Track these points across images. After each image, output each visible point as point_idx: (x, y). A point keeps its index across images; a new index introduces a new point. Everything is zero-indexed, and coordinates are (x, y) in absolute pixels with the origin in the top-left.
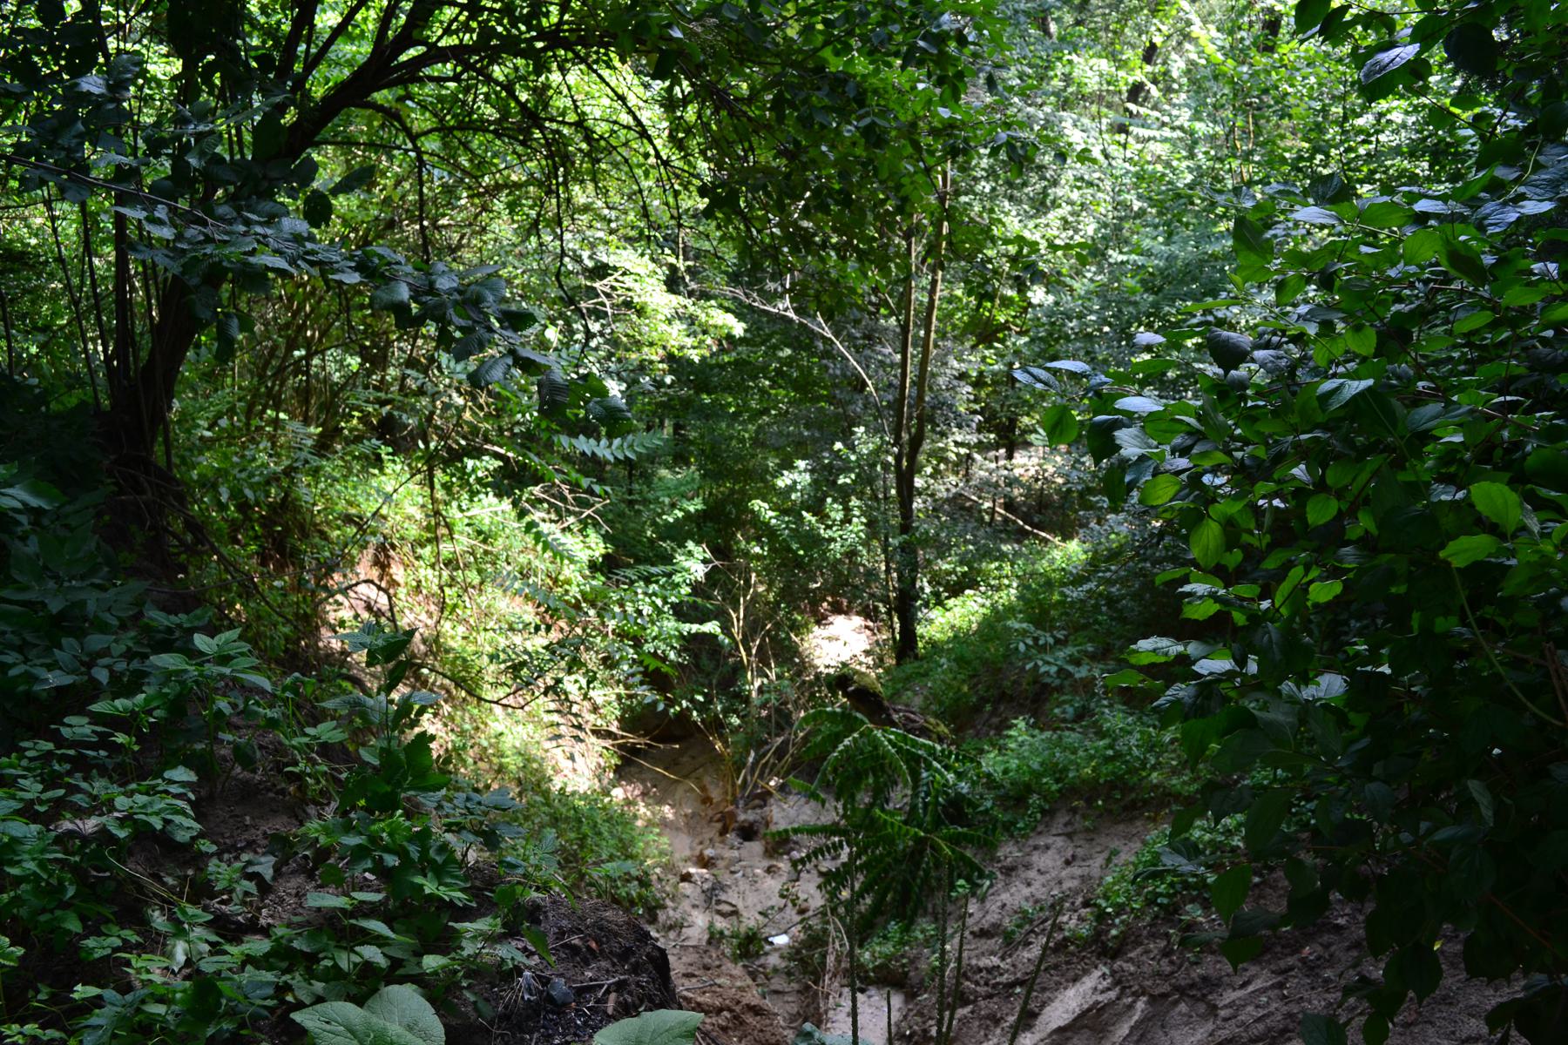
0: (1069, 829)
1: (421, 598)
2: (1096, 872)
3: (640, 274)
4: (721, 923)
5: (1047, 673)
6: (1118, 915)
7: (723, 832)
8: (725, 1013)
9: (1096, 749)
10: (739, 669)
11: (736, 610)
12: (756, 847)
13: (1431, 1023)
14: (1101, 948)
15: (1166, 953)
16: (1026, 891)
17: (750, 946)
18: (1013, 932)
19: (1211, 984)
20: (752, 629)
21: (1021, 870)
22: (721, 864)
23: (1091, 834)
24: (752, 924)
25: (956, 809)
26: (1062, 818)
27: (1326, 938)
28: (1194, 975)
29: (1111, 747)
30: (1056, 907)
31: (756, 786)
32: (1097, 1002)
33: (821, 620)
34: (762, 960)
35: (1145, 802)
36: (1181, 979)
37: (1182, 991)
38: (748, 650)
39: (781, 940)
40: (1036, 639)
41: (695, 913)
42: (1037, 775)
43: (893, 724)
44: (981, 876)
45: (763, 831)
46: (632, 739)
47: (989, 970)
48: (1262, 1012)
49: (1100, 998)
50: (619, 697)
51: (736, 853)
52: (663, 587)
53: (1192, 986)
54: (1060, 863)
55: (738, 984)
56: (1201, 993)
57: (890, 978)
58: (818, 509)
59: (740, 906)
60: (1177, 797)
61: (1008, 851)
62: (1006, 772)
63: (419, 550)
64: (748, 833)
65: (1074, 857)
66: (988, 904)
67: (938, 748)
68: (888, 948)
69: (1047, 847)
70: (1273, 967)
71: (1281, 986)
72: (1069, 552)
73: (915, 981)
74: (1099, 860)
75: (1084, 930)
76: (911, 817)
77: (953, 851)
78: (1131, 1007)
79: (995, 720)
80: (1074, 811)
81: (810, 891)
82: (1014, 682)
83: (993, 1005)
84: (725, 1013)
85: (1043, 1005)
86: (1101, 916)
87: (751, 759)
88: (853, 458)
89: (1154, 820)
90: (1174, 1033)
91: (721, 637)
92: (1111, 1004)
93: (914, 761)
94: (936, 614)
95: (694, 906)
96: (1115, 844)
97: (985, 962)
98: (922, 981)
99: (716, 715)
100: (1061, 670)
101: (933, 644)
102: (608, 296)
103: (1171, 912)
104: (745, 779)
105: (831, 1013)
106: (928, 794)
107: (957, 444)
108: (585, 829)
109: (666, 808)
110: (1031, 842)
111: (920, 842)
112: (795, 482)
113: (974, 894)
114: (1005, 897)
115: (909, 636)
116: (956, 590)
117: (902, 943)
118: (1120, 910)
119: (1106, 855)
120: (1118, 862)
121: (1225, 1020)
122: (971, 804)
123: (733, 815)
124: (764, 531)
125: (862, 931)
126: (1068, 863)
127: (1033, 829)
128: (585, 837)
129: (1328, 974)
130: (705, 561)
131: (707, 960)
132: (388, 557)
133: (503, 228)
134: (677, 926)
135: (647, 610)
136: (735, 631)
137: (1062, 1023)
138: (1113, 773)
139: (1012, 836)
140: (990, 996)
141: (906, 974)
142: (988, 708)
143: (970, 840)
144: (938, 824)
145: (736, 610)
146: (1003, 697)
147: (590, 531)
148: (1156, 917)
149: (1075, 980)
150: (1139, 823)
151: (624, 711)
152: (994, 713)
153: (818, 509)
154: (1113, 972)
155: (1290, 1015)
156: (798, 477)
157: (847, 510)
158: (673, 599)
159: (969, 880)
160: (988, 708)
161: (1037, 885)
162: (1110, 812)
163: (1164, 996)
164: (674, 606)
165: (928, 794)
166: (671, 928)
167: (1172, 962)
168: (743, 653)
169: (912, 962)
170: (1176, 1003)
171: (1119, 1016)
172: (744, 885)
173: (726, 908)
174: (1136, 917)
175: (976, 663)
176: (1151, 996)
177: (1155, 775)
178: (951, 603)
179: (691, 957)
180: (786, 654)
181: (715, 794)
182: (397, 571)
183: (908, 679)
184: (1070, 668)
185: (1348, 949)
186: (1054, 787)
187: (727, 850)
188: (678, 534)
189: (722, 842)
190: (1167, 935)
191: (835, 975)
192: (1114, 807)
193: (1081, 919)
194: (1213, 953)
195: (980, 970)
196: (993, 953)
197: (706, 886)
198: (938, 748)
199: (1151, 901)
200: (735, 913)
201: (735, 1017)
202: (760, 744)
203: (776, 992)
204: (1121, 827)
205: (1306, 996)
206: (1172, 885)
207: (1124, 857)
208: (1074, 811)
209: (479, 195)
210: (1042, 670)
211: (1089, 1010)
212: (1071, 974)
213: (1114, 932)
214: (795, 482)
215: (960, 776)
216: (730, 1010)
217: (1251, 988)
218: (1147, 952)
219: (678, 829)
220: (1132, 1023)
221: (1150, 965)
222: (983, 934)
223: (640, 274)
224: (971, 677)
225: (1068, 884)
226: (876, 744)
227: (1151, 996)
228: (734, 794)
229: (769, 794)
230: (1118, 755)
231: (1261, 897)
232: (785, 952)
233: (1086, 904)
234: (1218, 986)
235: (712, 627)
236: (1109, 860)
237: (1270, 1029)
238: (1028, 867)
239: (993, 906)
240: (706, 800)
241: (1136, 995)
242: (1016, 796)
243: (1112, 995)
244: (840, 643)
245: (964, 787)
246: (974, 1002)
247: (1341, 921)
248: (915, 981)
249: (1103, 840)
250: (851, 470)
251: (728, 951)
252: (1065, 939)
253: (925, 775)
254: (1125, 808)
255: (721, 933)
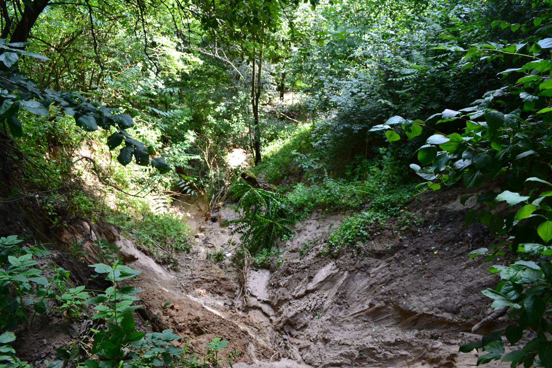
0: (317, 218)
1: (103, 154)
2: (327, 231)
3: (168, 45)
4: (210, 251)
5: (305, 168)
6: (336, 245)
7: (206, 220)
8: (215, 282)
9: (325, 193)
10: (207, 169)
11: (205, 151)
12: (217, 224)
13: (436, 276)
14: (332, 256)
15: (352, 257)
16: (305, 238)
17: (219, 257)
18: (302, 251)
19: (367, 266)
20: (211, 155)
21: (303, 231)
22: (206, 230)
23: (324, 219)
24: (219, 250)
25: (281, 213)
26: (315, 214)
27: (402, 251)
28: (362, 264)
29: (329, 192)
30: (315, 243)
31: (215, 205)
32: (332, 273)
33: (231, 151)
34: (223, 262)
35: (341, 209)
36: (358, 265)
37: (359, 269)
38: (210, 163)
39: (229, 255)
40: (301, 157)
41: (201, 248)
42: (306, 201)
43: (260, 187)
44: (291, 233)
45: (218, 219)
46: (175, 193)
47: (296, 264)
48: (384, 275)
49: (333, 272)
50: (170, 181)
51: (211, 227)
52: (181, 145)
53: (362, 267)
54: (315, 228)
55: (218, 272)
56: (365, 269)
57: (265, 266)
58: (229, 118)
59: (215, 244)
60: (352, 208)
61: (298, 225)
62: (296, 200)
63: (101, 139)
64: (214, 220)
65: (319, 226)
66: (294, 242)
67: (274, 194)
68: (263, 257)
69: (311, 224)
70: (386, 260)
71: (389, 266)
72: (305, 127)
73: (273, 267)
74: (328, 227)
75: (326, 250)
76: (267, 216)
77: (282, 226)
78: (343, 274)
79: (288, 181)
80: (319, 212)
81: (236, 238)
82: (293, 169)
83: (299, 275)
84: (215, 282)
85: (315, 274)
86: (331, 246)
87: (213, 197)
88: (239, 101)
89: (344, 214)
90: (357, 282)
91: (201, 160)
92: (336, 274)
93: (267, 199)
94: (266, 148)
95: (200, 245)
96: (332, 222)
97: (295, 261)
98: (275, 267)
99: (201, 184)
100: (309, 167)
101: (266, 157)
102: (158, 53)
103: (353, 244)
104: (212, 204)
105: (248, 279)
106: (272, 209)
107: (269, 95)
108: (165, 228)
109: (188, 213)
110: (306, 222)
111: (270, 223)
112: (221, 110)
113: (289, 239)
114: (299, 240)
115: (258, 155)
116: (271, 140)
117: (268, 255)
118: (337, 244)
119: (329, 225)
120: (336, 227)
121: (373, 277)
122: (286, 211)
123: (209, 215)
124: (210, 126)
125: (253, 251)
126: (318, 228)
127: (306, 218)
128: (166, 230)
129: (403, 262)
130: (194, 136)
131: (207, 265)
132: (91, 142)
133: (122, 32)
134: (196, 253)
135: (177, 152)
136: (205, 158)
137: (321, 280)
138: (330, 200)
139: (299, 220)
140: (298, 272)
141: (270, 265)
142: (286, 177)
143: (286, 222)
144: (276, 218)
145: (205, 151)
146: (290, 174)
147: (156, 128)
148: (348, 246)
149: (324, 266)
150: (339, 215)
151: (172, 185)
152: (287, 179)
153: (229, 118)
154: (336, 264)
155: (392, 275)
156: (221, 108)
157: (238, 118)
158: (185, 149)
159: (287, 235)
160: (286, 177)
161: (308, 235)
162: (330, 212)
163: (353, 271)
164: (185, 151)
165: (272, 209)
166: (194, 253)
167: (354, 260)
168: (208, 164)
169: (271, 261)
170: (357, 273)
171: (339, 277)
172: (215, 238)
173: (210, 245)
174: (342, 246)
175: (281, 164)
176: (349, 271)
177: (343, 200)
178: (270, 143)
179: (202, 264)
180: (221, 163)
181: (203, 208)
182: (95, 146)
183: (260, 169)
184: (313, 166)
185: (409, 254)
186: (312, 205)
187: (209, 225)
188: (184, 128)
189: (206, 223)
190: (352, 252)
191: (248, 267)
192: (331, 210)
193: (324, 247)
194: (367, 256)
195: (294, 264)
196: (297, 258)
197: (203, 239)
198: (274, 194)
199: (347, 241)
200: (213, 247)
201: (218, 282)
202: (216, 192)
203: (229, 271)
204: (334, 216)
205: (397, 269)
206: (353, 236)
207: (335, 226)
208: (319, 212)
209: (112, 20)
210: (304, 167)
211: (330, 276)
212: (323, 264)
213: (335, 251)
214: (221, 110)
215: (282, 202)
216: (216, 280)
217: (380, 267)
218: (346, 257)
219: (192, 220)
220: (344, 279)
221: (347, 261)
222: (293, 251)
223: (168, 45)
224: (280, 168)
225: (318, 235)
226: (254, 194)
227: (349, 271)
228: (209, 208)
229: (220, 207)
230: (332, 195)
231: (380, 238)
232: (231, 258)
233: (325, 242)
234: (369, 267)
235: (197, 157)
236: (330, 227)
237: (386, 280)
238: (305, 230)
239: (295, 242)
240: (200, 210)
241: (344, 271)
242: (300, 208)
243: (337, 271)
244: (237, 159)
245: (283, 206)
246: (293, 274)
247: (406, 245)
248: (273, 267)
249: (328, 221)
250: (239, 105)
251: (213, 260)
252: (320, 253)
253: (271, 203)
254: (334, 211)
255: (210, 255)
